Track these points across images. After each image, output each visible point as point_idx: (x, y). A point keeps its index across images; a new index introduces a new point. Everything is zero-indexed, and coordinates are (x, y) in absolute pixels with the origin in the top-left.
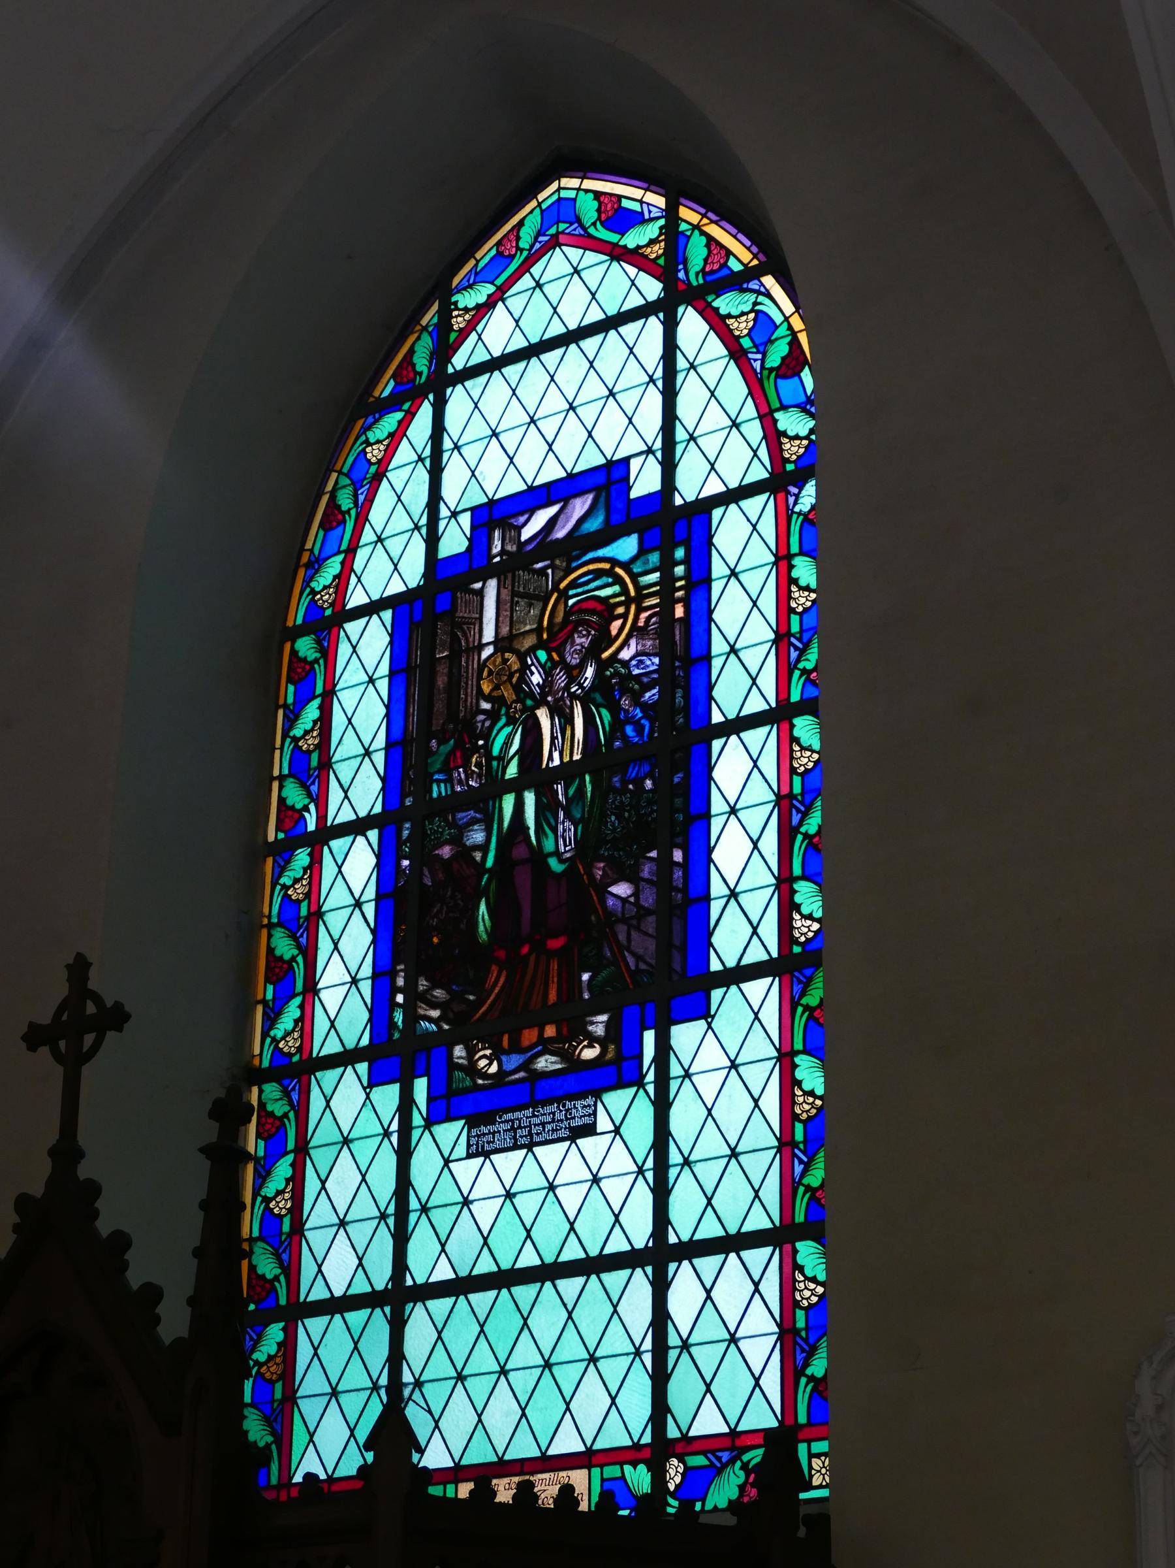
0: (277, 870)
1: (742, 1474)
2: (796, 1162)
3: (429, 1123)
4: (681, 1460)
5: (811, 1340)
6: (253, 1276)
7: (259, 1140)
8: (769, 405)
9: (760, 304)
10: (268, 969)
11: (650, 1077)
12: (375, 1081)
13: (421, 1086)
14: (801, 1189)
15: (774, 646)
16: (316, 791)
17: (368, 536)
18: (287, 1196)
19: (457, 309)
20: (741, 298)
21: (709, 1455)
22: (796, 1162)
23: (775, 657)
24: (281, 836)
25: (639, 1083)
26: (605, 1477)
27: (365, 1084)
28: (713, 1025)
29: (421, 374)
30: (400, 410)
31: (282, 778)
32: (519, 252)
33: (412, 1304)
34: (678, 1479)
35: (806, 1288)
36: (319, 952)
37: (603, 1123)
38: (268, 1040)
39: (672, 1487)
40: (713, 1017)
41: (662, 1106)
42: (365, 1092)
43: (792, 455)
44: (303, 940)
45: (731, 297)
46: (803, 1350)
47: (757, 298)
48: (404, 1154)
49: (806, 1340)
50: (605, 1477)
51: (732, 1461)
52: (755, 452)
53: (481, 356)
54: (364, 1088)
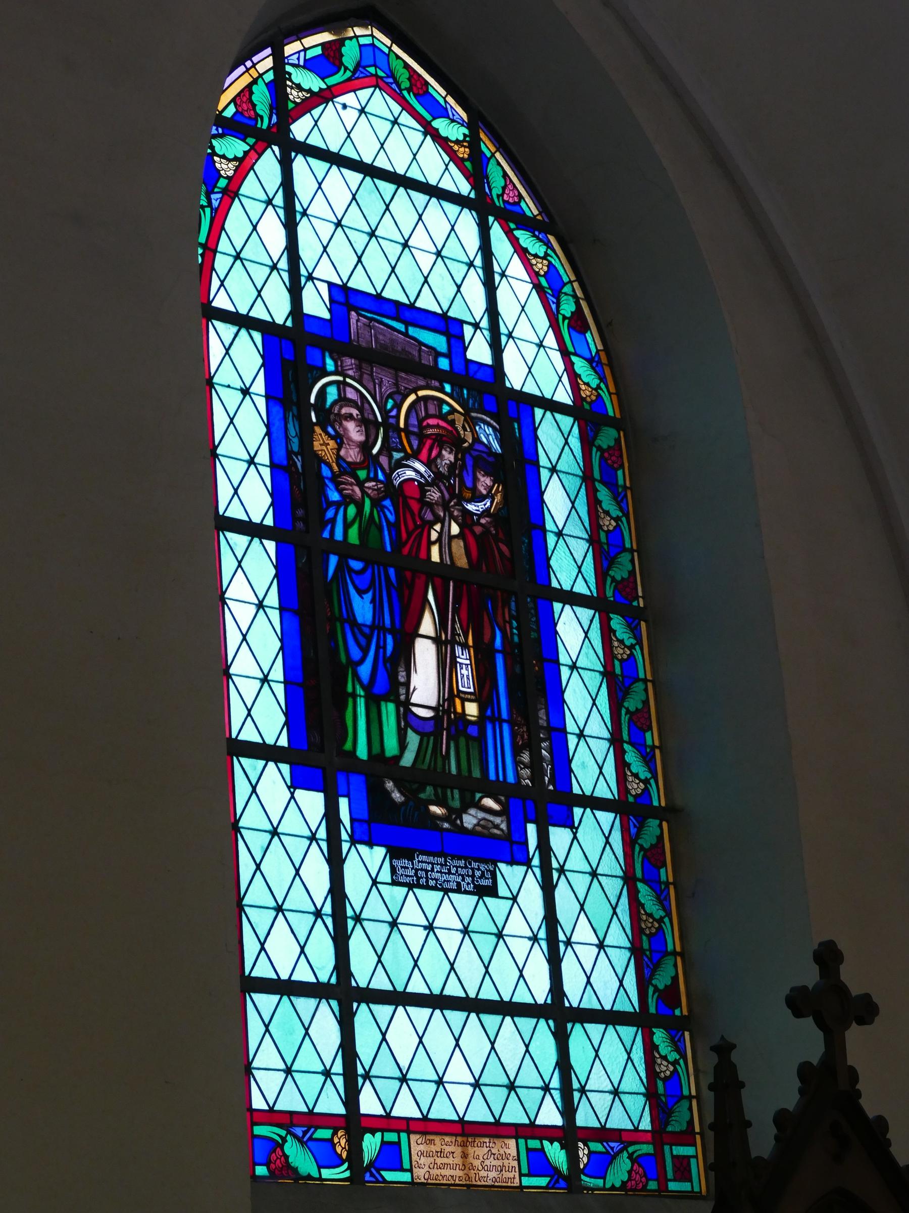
1: (628, 1162)
3: (354, 841)
4: (585, 1144)
9: (345, 72)
11: (536, 861)
12: (297, 783)
17: (551, 341)
20: (612, 1171)
25: (527, 862)
26: (389, 881)
27: (289, 784)
29: (465, 135)
30: (244, 140)
32: (549, 258)
37: (502, 890)
39: (582, 1166)
40: (577, 828)
43: (339, 1139)
45: (616, 1168)
47: (350, 70)
48: (335, 862)
51: (621, 1151)
53: (315, 141)
54: (289, 788)
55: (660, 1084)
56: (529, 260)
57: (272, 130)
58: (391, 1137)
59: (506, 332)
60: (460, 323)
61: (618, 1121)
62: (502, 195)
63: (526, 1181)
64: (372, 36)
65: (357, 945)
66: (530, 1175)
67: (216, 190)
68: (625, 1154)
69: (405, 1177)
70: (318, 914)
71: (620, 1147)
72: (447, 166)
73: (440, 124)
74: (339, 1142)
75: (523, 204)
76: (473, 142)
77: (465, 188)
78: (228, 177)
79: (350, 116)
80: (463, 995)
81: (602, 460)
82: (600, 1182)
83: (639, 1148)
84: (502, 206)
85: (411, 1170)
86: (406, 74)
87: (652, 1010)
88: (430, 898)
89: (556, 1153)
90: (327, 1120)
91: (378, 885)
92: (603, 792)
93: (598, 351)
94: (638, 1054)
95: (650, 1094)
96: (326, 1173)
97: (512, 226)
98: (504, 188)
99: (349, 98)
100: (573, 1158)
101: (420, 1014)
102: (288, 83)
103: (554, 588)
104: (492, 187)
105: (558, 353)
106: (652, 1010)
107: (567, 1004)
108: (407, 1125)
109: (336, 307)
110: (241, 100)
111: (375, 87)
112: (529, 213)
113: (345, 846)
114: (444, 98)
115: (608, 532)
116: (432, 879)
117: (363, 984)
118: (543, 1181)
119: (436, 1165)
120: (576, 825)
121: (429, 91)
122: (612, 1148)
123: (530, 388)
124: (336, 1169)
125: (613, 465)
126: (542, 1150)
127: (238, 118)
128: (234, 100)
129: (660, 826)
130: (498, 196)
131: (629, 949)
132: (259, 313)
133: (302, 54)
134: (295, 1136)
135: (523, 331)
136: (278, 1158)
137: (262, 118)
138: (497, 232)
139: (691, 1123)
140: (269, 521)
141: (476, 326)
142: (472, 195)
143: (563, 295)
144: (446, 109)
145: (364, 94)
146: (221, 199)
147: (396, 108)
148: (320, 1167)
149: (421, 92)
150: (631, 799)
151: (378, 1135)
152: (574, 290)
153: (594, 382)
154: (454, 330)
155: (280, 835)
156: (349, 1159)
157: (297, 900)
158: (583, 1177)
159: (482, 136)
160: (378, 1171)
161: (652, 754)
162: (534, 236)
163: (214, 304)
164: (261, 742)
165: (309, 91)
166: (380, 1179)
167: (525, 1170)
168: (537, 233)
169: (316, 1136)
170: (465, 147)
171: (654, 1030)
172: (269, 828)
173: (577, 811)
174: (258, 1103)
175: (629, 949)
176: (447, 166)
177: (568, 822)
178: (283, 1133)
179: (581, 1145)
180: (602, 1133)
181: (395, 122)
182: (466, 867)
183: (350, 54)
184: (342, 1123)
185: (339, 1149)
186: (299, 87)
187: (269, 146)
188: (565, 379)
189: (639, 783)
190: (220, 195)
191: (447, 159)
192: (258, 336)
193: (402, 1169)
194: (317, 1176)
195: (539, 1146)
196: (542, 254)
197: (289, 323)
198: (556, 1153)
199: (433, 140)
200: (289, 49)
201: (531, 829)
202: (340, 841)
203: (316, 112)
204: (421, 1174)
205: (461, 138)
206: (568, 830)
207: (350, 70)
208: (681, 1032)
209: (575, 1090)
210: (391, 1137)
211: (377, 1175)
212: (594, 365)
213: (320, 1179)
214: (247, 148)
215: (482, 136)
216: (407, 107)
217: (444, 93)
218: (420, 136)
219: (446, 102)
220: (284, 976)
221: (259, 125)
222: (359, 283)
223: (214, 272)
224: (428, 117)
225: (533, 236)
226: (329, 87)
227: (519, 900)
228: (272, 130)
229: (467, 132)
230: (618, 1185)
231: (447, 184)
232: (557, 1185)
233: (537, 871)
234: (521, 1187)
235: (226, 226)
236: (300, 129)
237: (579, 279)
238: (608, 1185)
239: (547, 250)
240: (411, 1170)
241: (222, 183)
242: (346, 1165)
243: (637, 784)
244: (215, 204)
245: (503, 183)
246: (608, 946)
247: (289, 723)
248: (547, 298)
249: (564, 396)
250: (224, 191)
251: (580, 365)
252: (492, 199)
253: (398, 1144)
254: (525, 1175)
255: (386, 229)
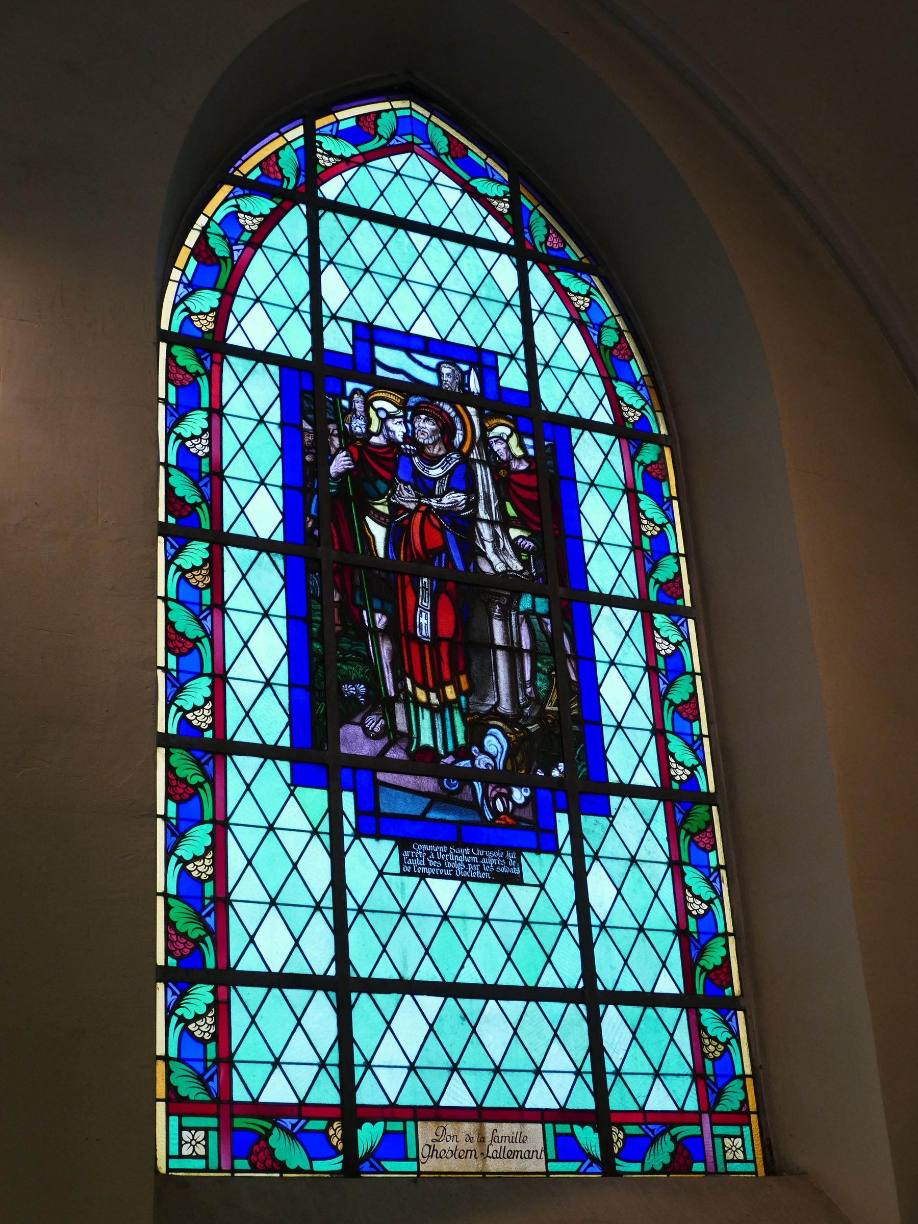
0: (172, 690)
2: (710, 1092)
3: (358, 834)
4: (621, 1128)
5: (702, 941)
6: (172, 777)
7: (169, 802)
8: (606, 316)
10: (167, 639)
11: (567, 849)
12: (298, 780)
13: (348, 800)
14: (667, 703)
15: (670, 869)
16: (209, 493)
17: (592, 368)
18: (207, 862)
19: (321, 148)
21: (643, 1127)
22: (710, 1092)
23: (671, 882)
24: (172, 520)
26: (398, 872)
27: (289, 782)
28: (614, 823)
31: (166, 1058)
33: (323, 211)
34: (620, 1144)
35: (710, 1044)
36: (225, 573)
37: (528, 877)
38: (174, 1019)
39: (616, 1151)
40: (614, 817)
41: (580, 877)
42: (290, 789)
44: (210, 921)
46: (713, 1092)
47: (385, 138)
48: (337, 856)
49: (715, 1084)
50: (398, 872)
51: (662, 1134)
52: (601, 401)
53: (345, 199)
54: (288, 785)
55: (709, 1065)
56: (569, 297)
57: (299, 190)
58: (396, 1126)
59: (543, 362)
60: (495, 354)
61: (660, 1102)
62: (546, 242)
63: (553, 1167)
64: (411, 108)
65: (603, 953)
66: (557, 1160)
67: (239, 242)
68: (668, 1137)
69: (411, 1166)
70: (564, 924)
71: (660, 1130)
72: (485, 219)
73: (481, 185)
74: (335, 1134)
75: (567, 249)
76: (514, 199)
77: (503, 237)
78: (252, 231)
79: (383, 179)
80: (480, 982)
81: (645, 474)
82: (636, 1167)
83: (679, 1131)
84: (545, 252)
85: (417, 1159)
86: (445, 141)
87: (700, 991)
88: (445, 889)
89: (588, 1137)
90: (320, 1111)
91: (385, 876)
92: (643, 779)
93: (642, 377)
94: (667, 893)
95: (698, 1075)
96: (319, 1166)
97: (553, 268)
98: (547, 236)
99: (383, 163)
100: (606, 1142)
101: (514, 1007)
102: (319, 150)
103: (592, 592)
104: (534, 235)
105: (599, 379)
106: (700, 991)
107: (600, 987)
108: (417, 1114)
109: (359, 344)
110: (268, 164)
111: (412, 152)
112: (574, 258)
113: (347, 841)
114: (485, 161)
115: (651, 538)
116: (407, 865)
117: (364, 974)
118: (574, 1166)
119: (435, 1152)
120: (613, 814)
121: (469, 154)
122: (652, 1131)
123: (567, 410)
124: (333, 1160)
125: (658, 477)
126: (572, 1135)
127: (263, 179)
128: (260, 165)
129: (710, 812)
130: (541, 243)
131: (673, 932)
132: (277, 348)
133: (335, 125)
134: (283, 1129)
135: (561, 359)
136: (261, 1150)
137: (288, 179)
138: (537, 277)
139: (744, 1102)
140: (279, 536)
141: (512, 357)
142: (512, 243)
143: (605, 328)
144: (486, 170)
145: (399, 159)
146: (244, 250)
147: (433, 170)
148: (311, 1159)
149: (460, 155)
150: (675, 786)
151: (380, 1125)
152: (617, 323)
153: (639, 404)
154: (488, 360)
155: (276, 830)
156: (343, 1152)
157: (294, 892)
158: (617, 1161)
159: (522, 190)
160: (378, 1160)
161: (699, 742)
162: (576, 276)
163: (229, 342)
164: (260, 742)
165: (341, 157)
166: (381, 1170)
167: (552, 1155)
168: (579, 274)
169: (307, 1127)
170: (507, 202)
171: (655, 615)
172: (628, 856)
173: (614, 801)
174: (239, 1094)
175: (673, 932)
176: (485, 219)
177: (604, 811)
178: (268, 1125)
179: (615, 1129)
180: (643, 1115)
181: (432, 182)
182: (471, 855)
183: (386, 125)
184: (337, 1113)
185: (334, 1141)
186: (330, 154)
187: (297, 203)
188: (606, 402)
189: (701, 904)
190: (242, 247)
191: (485, 213)
192: (274, 369)
193: (406, 1159)
194: (308, 1168)
195: (569, 1131)
196: (584, 292)
197: (309, 358)
198: (588, 1137)
199: (471, 197)
200: (319, 123)
201: (562, 822)
202: (342, 835)
203: (347, 175)
204: (430, 1165)
205: (501, 194)
206: (605, 818)
207: (385, 138)
208: (732, 1012)
209: (609, 1073)
210: (396, 1126)
211: (377, 1165)
212: (639, 388)
213: (311, 1171)
214: (274, 205)
215: (522, 190)
216: (443, 168)
217: (484, 156)
218: (458, 194)
219: (486, 163)
220: (449, 979)
221: (284, 186)
222: (386, 321)
223: (231, 313)
224: (466, 177)
225: (575, 277)
226: (361, 154)
227: (376, 873)
228: (299, 190)
229: (507, 189)
230: (659, 1167)
231: (484, 234)
232: (589, 1170)
233: (569, 860)
234: (548, 1173)
235: (234, 309)
236: (330, 190)
237: (624, 313)
238: (647, 1168)
239: (590, 288)
240: (417, 1159)
241: (246, 237)
242: (341, 1158)
243: (699, 905)
244: (236, 255)
245: (545, 232)
246: (610, 927)
247: (291, 723)
248: (588, 331)
249: (604, 416)
250: (246, 244)
251: (622, 389)
252: (535, 246)
253: (403, 1133)
254: (552, 1161)
255: (419, 273)
